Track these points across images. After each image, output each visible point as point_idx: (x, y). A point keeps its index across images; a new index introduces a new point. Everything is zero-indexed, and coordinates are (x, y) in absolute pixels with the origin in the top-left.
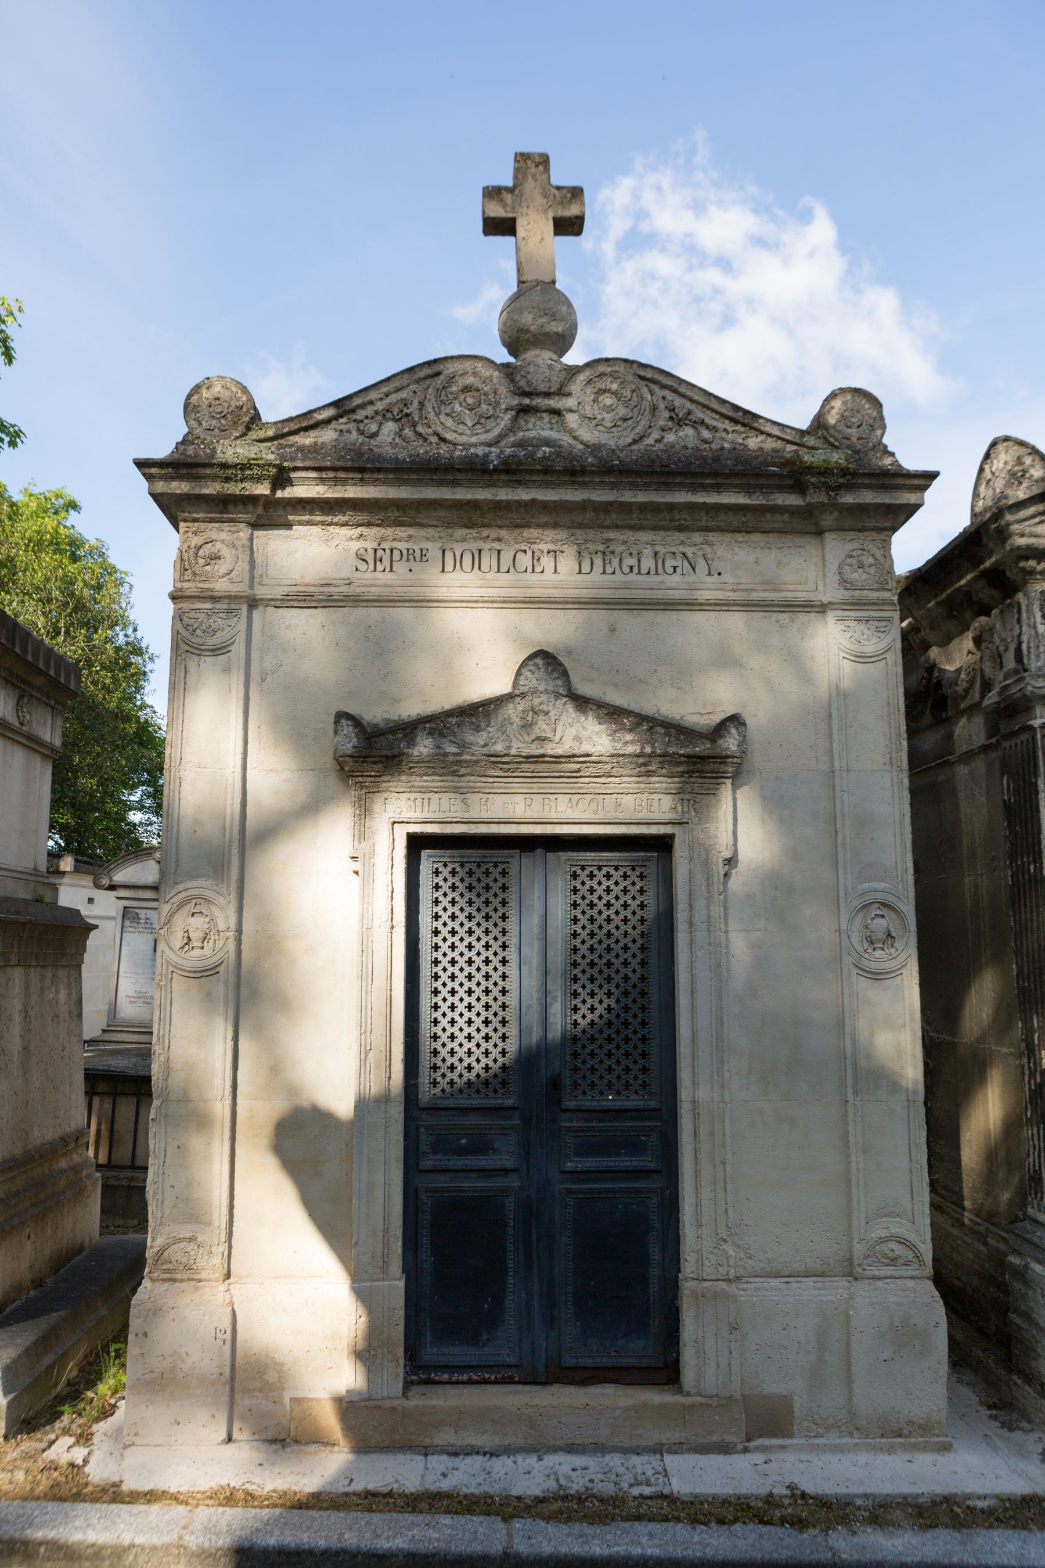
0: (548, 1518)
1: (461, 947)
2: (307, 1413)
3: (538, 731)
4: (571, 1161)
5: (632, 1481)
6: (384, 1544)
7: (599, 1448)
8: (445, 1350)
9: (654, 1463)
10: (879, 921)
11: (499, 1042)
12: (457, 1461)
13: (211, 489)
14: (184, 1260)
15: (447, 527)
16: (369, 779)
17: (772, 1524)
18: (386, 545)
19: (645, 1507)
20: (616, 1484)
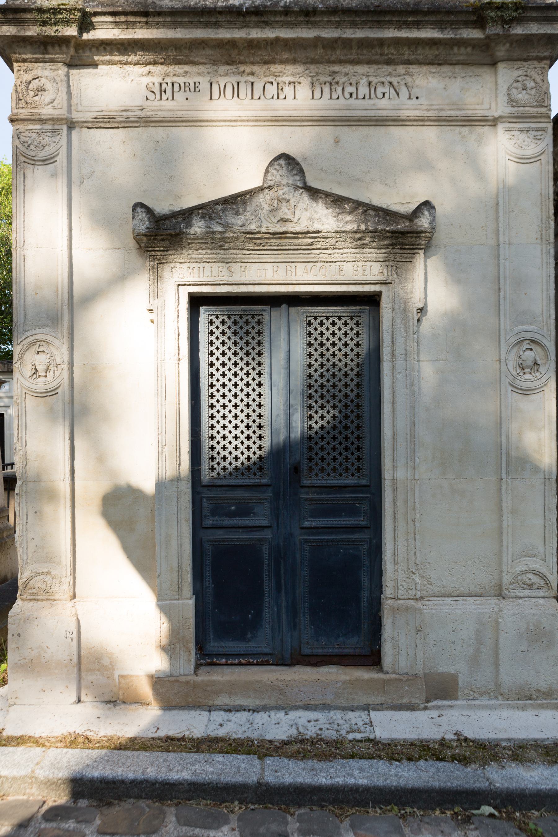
0: (289, 757)
1: (230, 375)
2: (130, 684)
3: (282, 214)
4: (308, 521)
5: (349, 730)
6: (174, 776)
7: (326, 707)
8: (222, 644)
9: (363, 717)
10: (528, 353)
11: (257, 440)
12: (231, 715)
13: (32, 31)
14: (43, 587)
15: (213, 64)
16: (160, 253)
17: (445, 761)
18: (169, 80)
19: (357, 748)
20: (337, 731)
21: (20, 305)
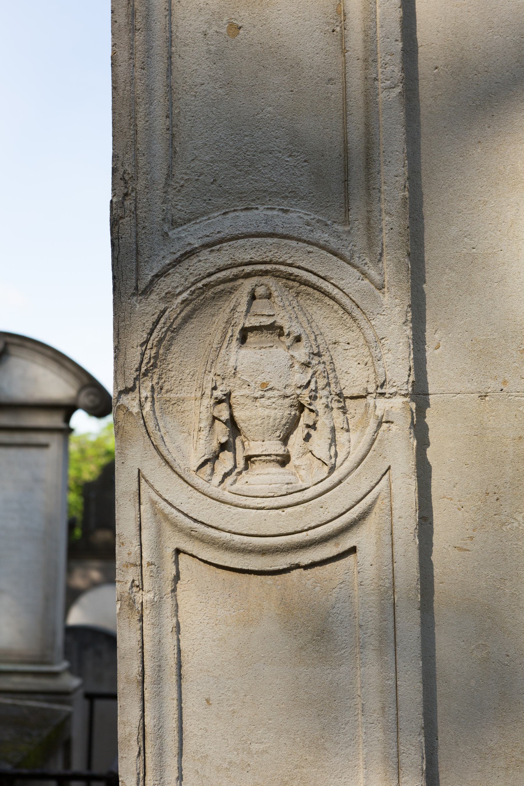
21: (149, 89)
